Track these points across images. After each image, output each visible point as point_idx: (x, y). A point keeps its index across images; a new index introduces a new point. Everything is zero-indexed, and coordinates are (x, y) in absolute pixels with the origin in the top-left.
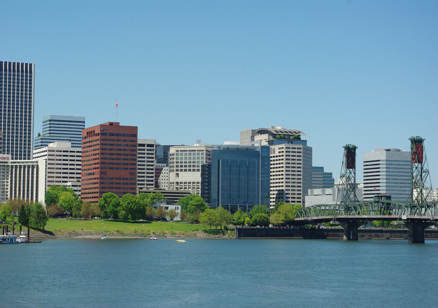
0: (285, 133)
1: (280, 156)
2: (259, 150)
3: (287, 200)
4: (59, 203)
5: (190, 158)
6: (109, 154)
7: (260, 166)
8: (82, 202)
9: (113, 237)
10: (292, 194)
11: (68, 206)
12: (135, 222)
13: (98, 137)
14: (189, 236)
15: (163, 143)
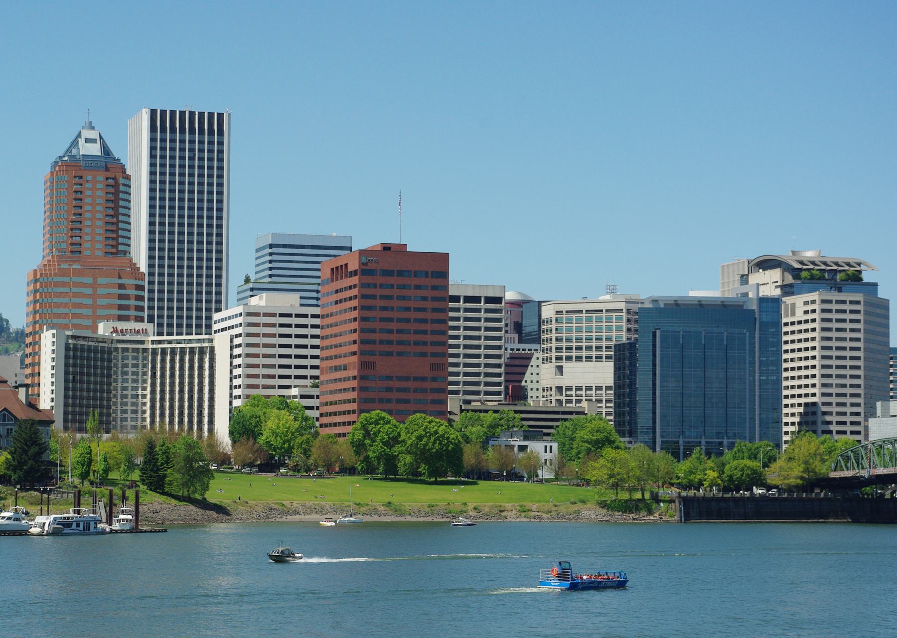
0: (823, 267)
1: (806, 321)
2: (755, 307)
3: (825, 428)
4: (264, 438)
5: (589, 330)
6: (382, 320)
7: (757, 345)
8: (317, 434)
9: (376, 518)
10: (838, 414)
11: (284, 444)
12: (436, 483)
13: (355, 280)
14: (563, 517)
15: (537, 299)
